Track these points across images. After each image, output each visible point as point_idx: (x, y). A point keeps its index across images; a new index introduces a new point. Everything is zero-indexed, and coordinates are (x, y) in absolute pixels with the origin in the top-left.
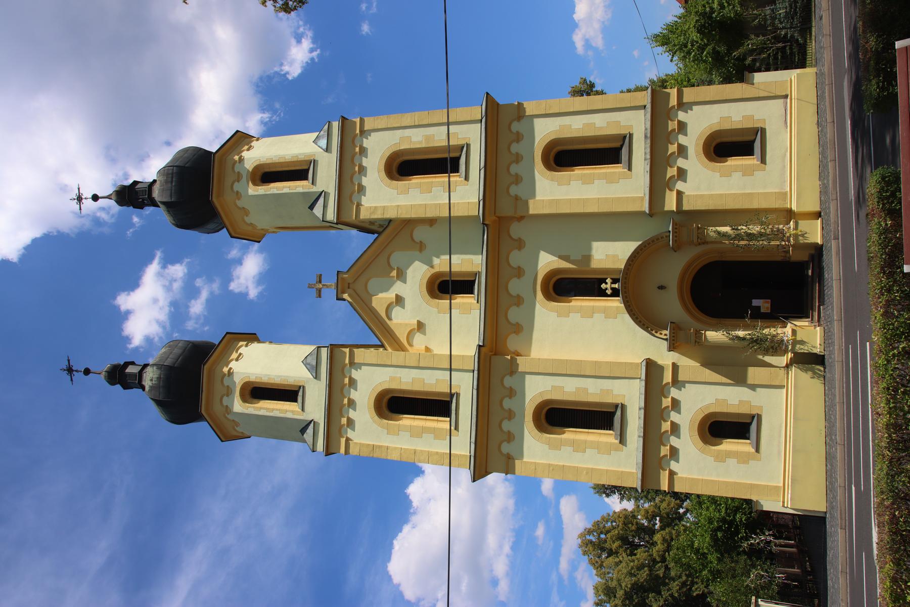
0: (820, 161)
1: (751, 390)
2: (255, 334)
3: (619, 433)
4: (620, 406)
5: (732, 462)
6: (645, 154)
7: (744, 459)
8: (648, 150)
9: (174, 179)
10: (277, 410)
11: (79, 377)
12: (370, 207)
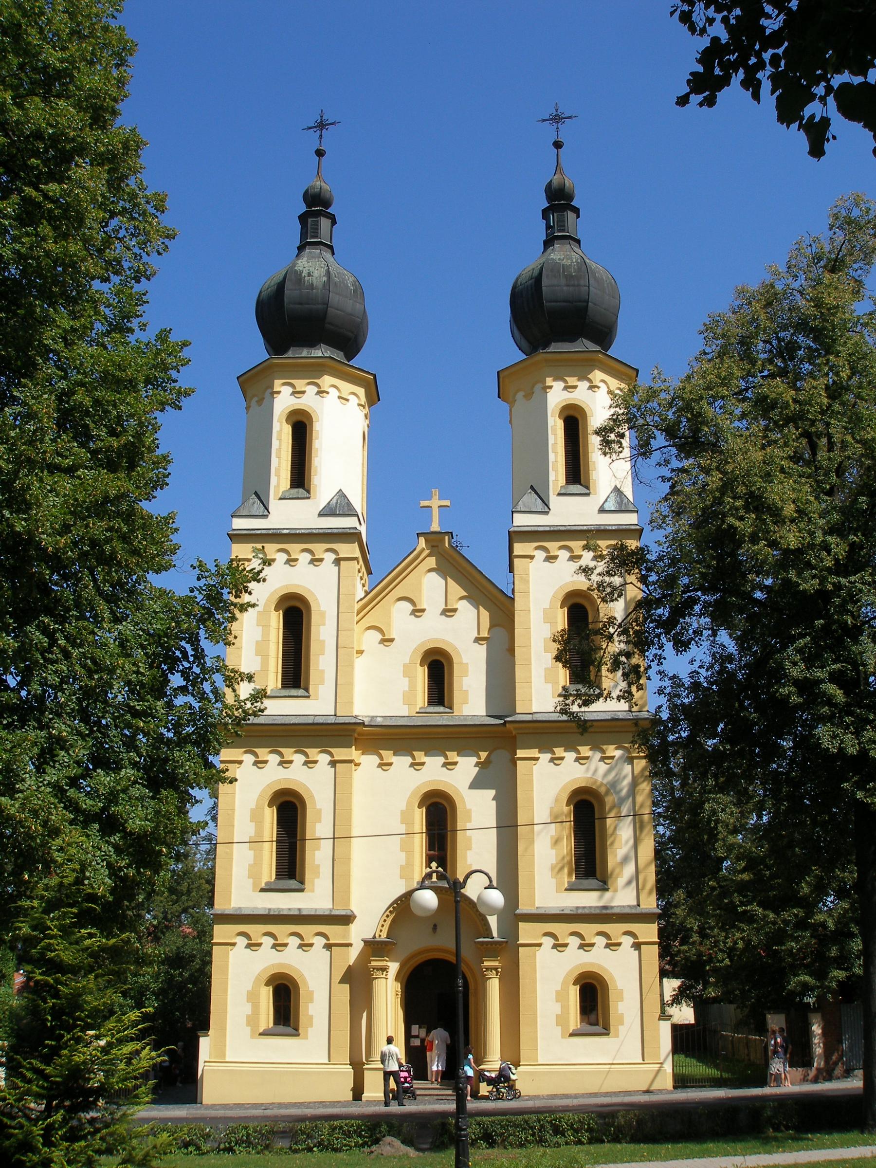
0: (339, 1102)
1: (471, 780)
2: (379, 400)
3: (273, 887)
4: (302, 887)
5: (248, 1009)
6: (584, 908)
7: (252, 1020)
8: (587, 911)
9: (571, 289)
10: (279, 463)
11: (312, 140)
12: (528, 575)
